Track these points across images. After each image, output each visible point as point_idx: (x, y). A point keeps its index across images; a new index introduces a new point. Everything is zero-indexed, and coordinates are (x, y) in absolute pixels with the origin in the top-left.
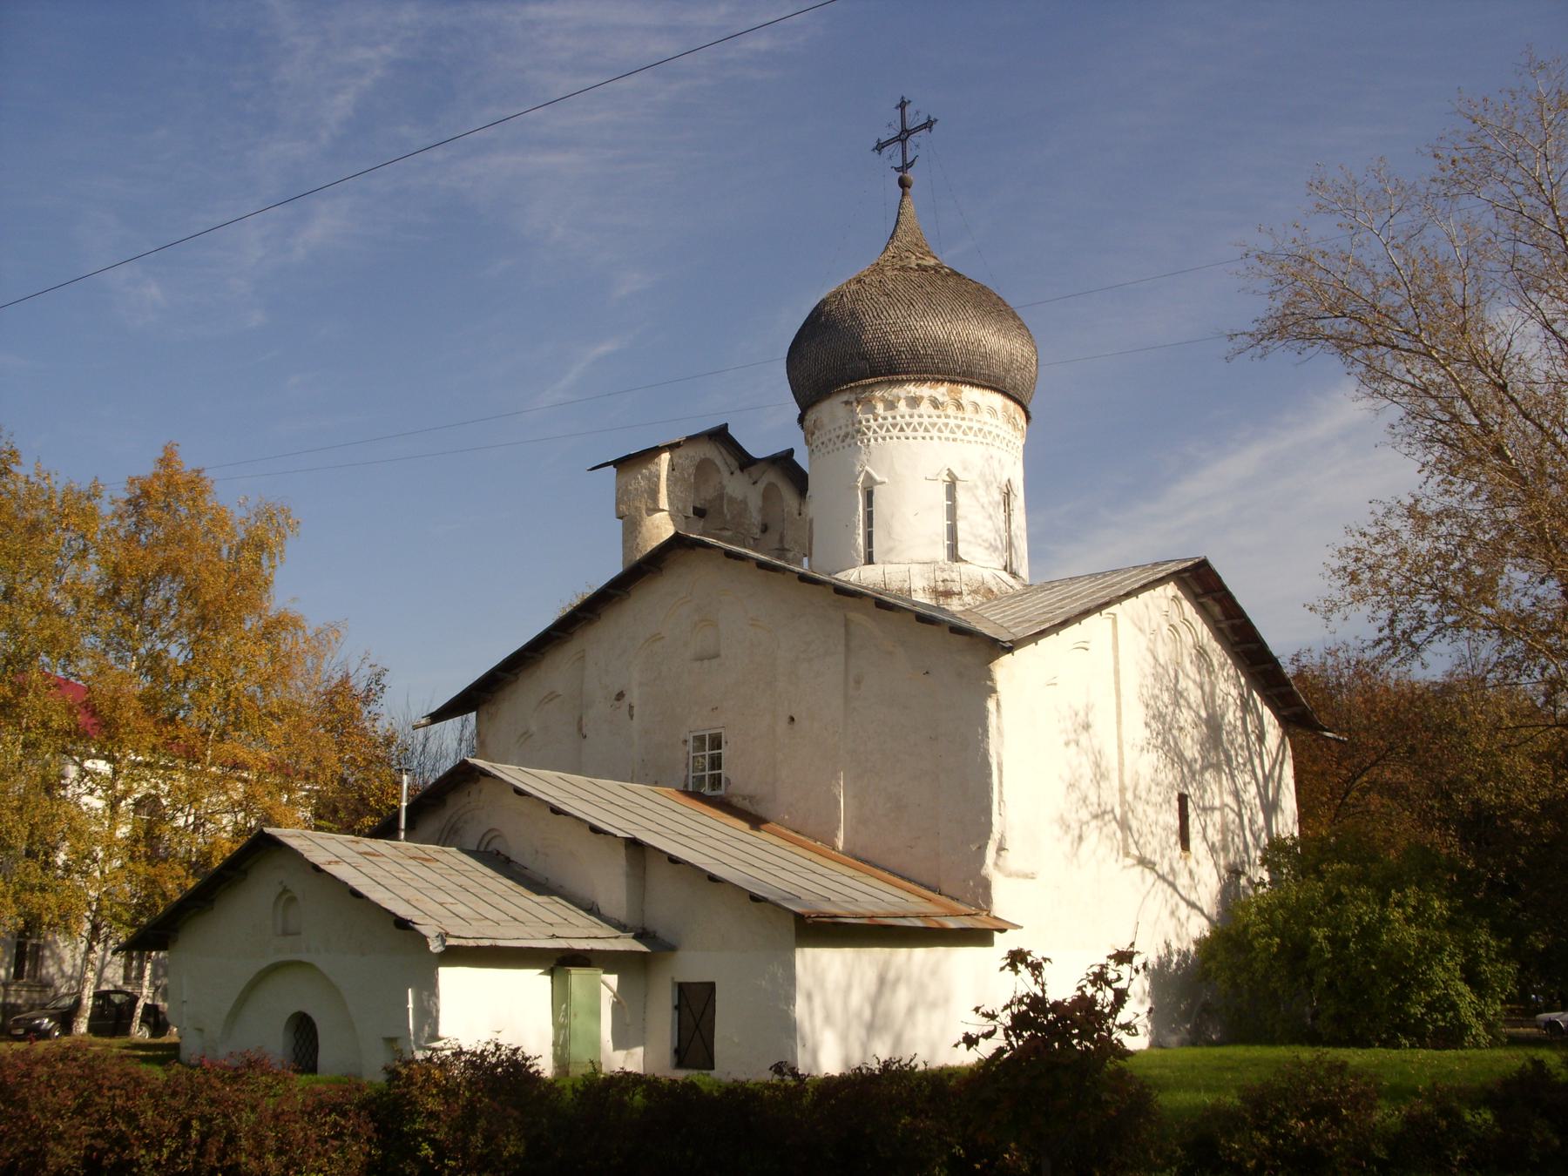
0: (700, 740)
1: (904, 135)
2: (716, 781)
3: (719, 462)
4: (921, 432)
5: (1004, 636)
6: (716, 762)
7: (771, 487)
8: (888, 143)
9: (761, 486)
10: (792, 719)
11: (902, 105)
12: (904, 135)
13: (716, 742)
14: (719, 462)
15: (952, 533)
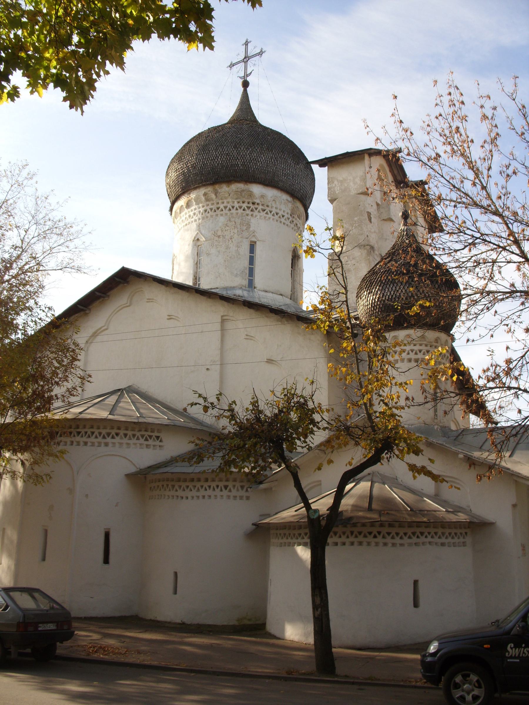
11: (246, 44)
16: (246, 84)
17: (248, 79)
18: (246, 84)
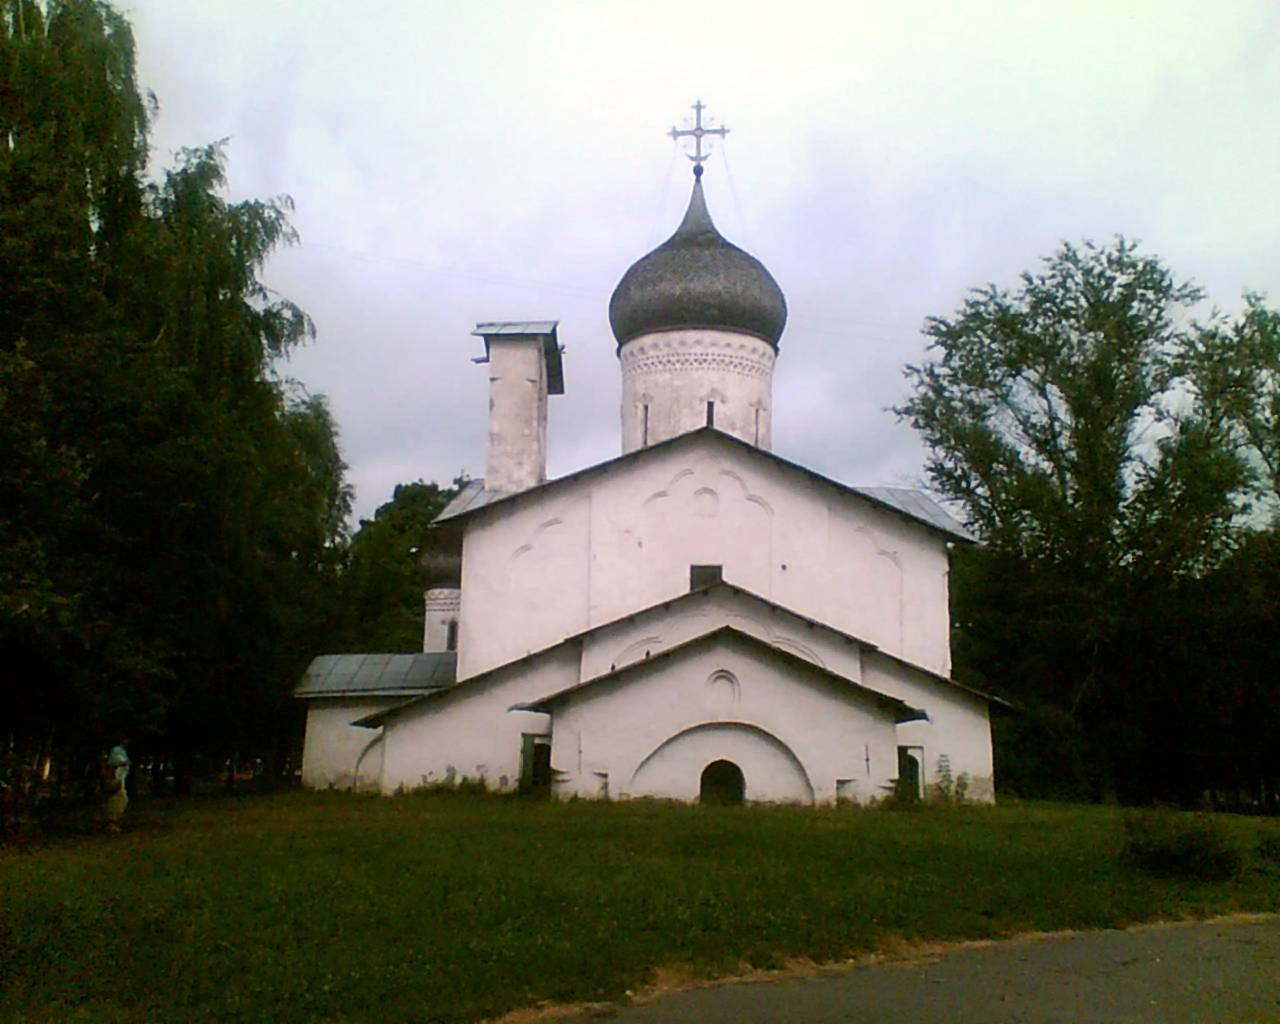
1: (699, 132)
8: (683, 133)
10: (784, 567)
11: (699, 107)
12: (699, 132)
16: (698, 171)
17: (702, 164)
18: (698, 171)
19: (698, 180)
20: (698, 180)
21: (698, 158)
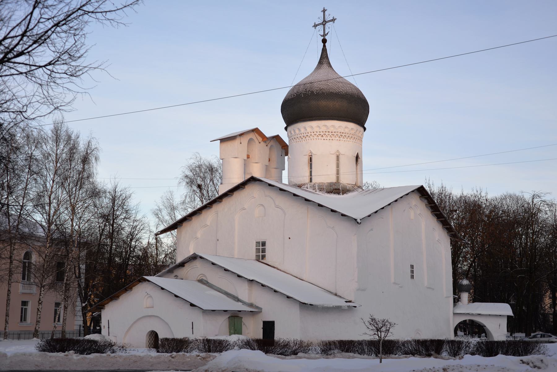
0: (258, 243)
1: (324, 23)
2: (264, 257)
3: (255, 138)
4: (329, 138)
5: (358, 216)
6: (264, 251)
7: (271, 146)
9: (269, 146)
11: (324, 11)
12: (324, 23)
13: (264, 244)
14: (255, 138)
15: (338, 173)
16: (324, 41)
17: (326, 37)
18: (324, 41)
19: (324, 46)
20: (324, 46)
21: (325, 35)
